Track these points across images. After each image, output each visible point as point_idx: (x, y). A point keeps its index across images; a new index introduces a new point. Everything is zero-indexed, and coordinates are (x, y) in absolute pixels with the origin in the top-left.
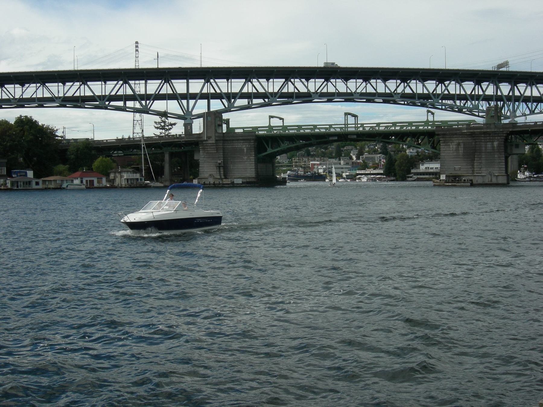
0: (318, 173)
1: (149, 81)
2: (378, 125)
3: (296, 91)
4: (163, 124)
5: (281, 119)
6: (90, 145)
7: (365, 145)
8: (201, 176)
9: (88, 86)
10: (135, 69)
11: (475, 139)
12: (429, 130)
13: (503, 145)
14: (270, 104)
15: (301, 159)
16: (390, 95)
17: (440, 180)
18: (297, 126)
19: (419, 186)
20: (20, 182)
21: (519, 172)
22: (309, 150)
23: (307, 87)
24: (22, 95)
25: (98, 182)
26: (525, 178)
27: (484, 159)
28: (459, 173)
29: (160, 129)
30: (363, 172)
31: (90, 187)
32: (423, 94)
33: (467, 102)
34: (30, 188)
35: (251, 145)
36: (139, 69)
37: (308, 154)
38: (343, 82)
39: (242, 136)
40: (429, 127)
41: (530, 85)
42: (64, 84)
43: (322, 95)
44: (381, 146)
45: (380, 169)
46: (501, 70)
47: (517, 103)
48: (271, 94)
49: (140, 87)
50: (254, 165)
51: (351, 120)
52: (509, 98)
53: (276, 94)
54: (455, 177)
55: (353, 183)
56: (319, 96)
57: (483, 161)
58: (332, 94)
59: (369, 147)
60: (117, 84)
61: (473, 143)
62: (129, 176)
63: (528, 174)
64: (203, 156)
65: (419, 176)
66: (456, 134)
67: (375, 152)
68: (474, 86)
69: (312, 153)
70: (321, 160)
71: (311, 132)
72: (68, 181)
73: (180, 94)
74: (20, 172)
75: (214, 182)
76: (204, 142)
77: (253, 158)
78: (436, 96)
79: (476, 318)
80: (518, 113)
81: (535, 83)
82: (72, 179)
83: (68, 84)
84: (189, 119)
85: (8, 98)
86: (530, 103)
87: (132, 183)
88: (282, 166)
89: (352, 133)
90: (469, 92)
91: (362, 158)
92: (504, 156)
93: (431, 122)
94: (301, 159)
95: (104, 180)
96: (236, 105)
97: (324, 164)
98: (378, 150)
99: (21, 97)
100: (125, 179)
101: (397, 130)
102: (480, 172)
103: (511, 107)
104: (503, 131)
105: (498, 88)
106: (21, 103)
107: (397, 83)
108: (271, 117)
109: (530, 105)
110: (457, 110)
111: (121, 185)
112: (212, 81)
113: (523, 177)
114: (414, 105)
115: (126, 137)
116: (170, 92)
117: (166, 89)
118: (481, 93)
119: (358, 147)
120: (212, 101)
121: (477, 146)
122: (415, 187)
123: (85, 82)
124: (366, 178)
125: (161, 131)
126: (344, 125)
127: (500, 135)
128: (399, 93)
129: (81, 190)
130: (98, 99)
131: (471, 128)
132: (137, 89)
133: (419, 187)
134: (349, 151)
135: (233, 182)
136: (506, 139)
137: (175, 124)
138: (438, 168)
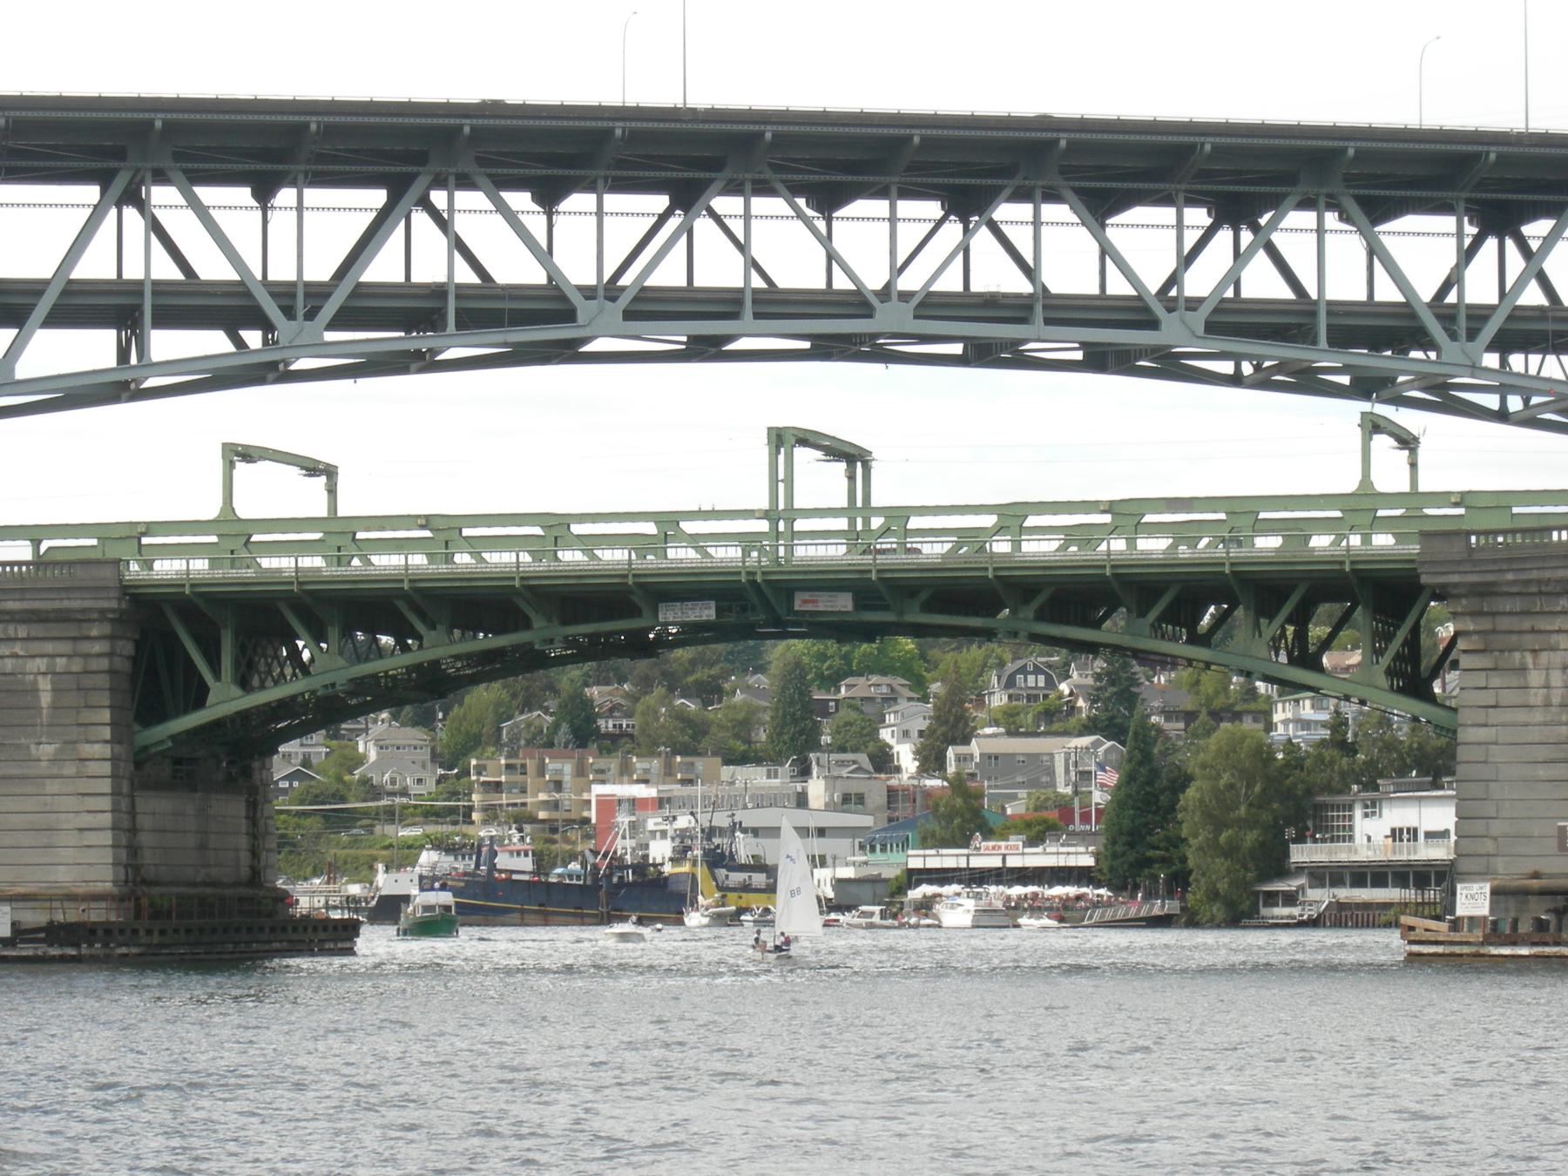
0: (642, 867)
2: (1012, 517)
5: (312, 468)
7: (984, 667)
9: (994, 228)
10: (623, 107)
12: (1382, 558)
14: (273, 365)
16: (1136, 312)
17: (1456, 925)
18: (427, 521)
19: (1078, 969)
22: (588, 704)
23: (544, 255)
30: (949, 859)
32: (1370, 307)
35: (86, 656)
38: (800, 215)
39: (21, 593)
40: (1383, 540)
44: (1098, 677)
45: (1083, 838)
48: (285, 294)
50: (106, 803)
53: (317, 294)
56: (629, 315)
58: (725, 304)
59: (1010, 683)
65: (1346, 894)
67: (1055, 717)
69: (606, 725)
70: (668, 772)
71: (638, 564)
78: (1462, 322)
88: (390, 815)
89: (824, 580)
96: (25, 369)
97: (688, 804)
98: (1073, 709)
99: (1229, 293)
107: (1180, 226)
108: (239, 454)
114: (1307, 382)
119: (936, 687)
124: (970, 904)
128: (1200, 300)
133: (1298, 969)
134: (867, 708)
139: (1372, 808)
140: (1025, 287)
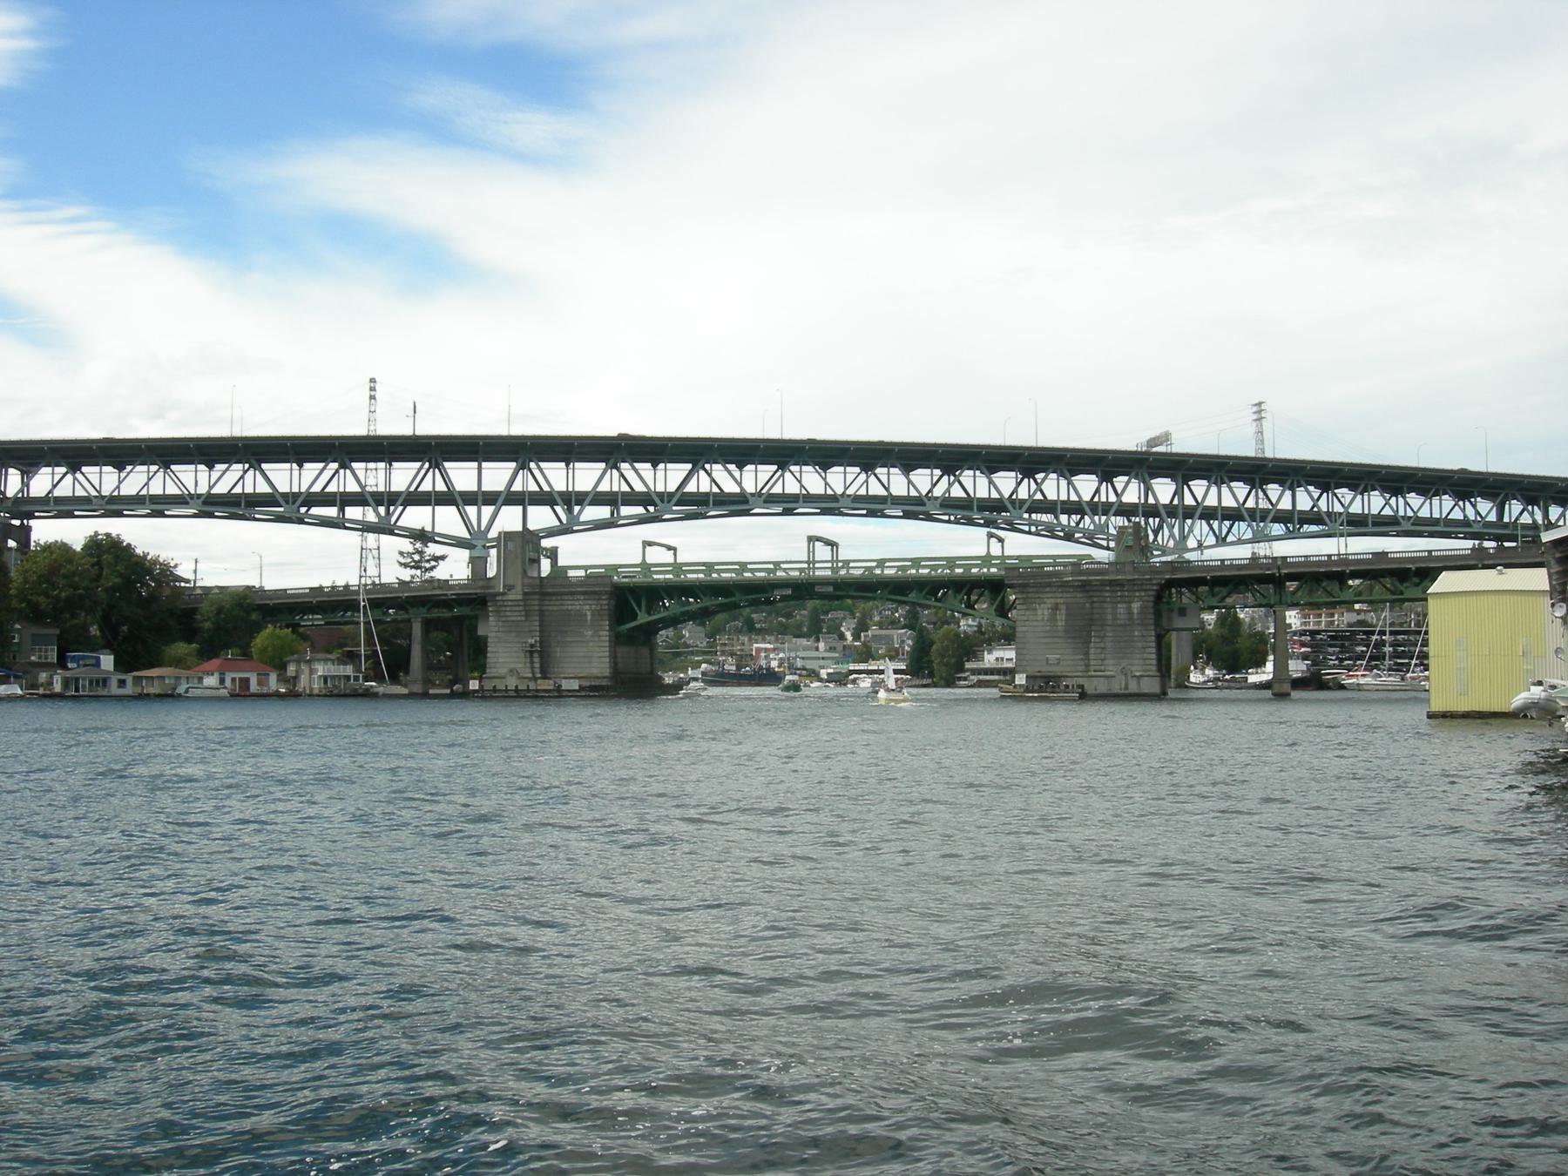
0: (768, 669)
1: (395, 465)
2: (881, 563)
3: (715, 490)
4: (417, 557)
5: (669, 548)
6: (248, 601)
8: (490, 672)
10: (368, 437)
11: (1091, 597)
13: (1151, 610)
15: (735, 638)
16: (919, 501)
17: (1015, 687)
18: (704, 564)
20: (84, 679)
21: (1192, 668)
23: (740, 484)
24: (118, 487)
25: (260, 683)
26: (1205, 682)
27: (1110, 639)
28: (1057, 670)
29: (412, 567)
30: (862, 666)
31: (242, 693)
33: (1082, 518)
34: (105, 693)
36: (1171, 454)
37: (750, 628)
38: (817, 471)
39: (581, 586)
40: (993, 570)
41: (1362, 494)
42: (211, 467)
43: (771, 499)
46: (1154, 450)
47: (1189, 521)
48: (661, 495)
49: (373, 476)
51: (823, 552)
52: (1171, 511)
53: (671, 495)
54: (1047, 679)
55: (841, 690)
56: (765, 502)
57: (1109, 645)
58: (794, 498)
59: (881, 613)
60: (324, 468)
61: (1088, 605)
62: (329, 670)
63: (1211, 672)
64: (496, 629)
65: (981, 677)
66: (1050, 585)
67: (894, 624)
68: (1096, 484)
69: (758, 626)
70: (777, 640)
72: (190, 680)
73: (462, 494)
74: (84, 658)
75: (517, 686)
76: (498, 598)
77: (605, 634)
79: (73, 971)
80: (1192, 543)
81: (1226, 480)
82: (200, 674)
83: (220, 467)
84: (480, 547)
85: (180, 493)
86: (1216, 522)
87: (334, 686)
88: (692, 653)
89: (824, 582)
90: (1086, 497)
91: (865, 636)
92: (1153, 633)
93: (996, 558)
94: (735, 638)
95: (273, 678)
96: (582, 518)
98: (899, 621)
99: (116, 493)
100: (320, 676)
101: (922, 576)
102: (1102, 668)
103: (1176, 530)
104: (1150, 579)
105: (1148, 489)
106: (115, 506)
108: (647, 544)
109: (1215, 524)
110: (1062, 534)
111: (311, 689)
112: (532, 465)
113: (1202, 679)
115: (341, 582)
116: (441, 486)
117: (432, 483)
118: (1112, 498)
119: (858, 615)
120: (531, 509)
121: (1095, 611)
122: (976, 700)
123: (347, 461)
124: (870, 680)
125: (413, 572)
126: (806, 562)
127: (1144, 587)
129: (220, 699)
130: (283, 503)
131: (1082, 573)
132: (371, 481)
135: (560, 686)
136: (1158, 598)
137: (443, 558)
138: (1012, 659)
139: (990, 652)
140: (886, 493)
